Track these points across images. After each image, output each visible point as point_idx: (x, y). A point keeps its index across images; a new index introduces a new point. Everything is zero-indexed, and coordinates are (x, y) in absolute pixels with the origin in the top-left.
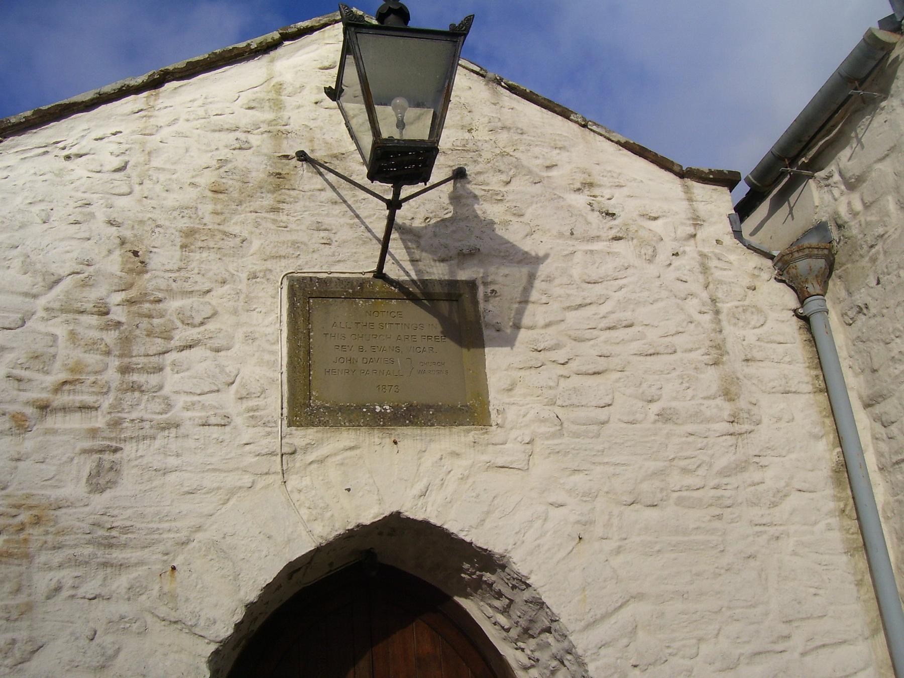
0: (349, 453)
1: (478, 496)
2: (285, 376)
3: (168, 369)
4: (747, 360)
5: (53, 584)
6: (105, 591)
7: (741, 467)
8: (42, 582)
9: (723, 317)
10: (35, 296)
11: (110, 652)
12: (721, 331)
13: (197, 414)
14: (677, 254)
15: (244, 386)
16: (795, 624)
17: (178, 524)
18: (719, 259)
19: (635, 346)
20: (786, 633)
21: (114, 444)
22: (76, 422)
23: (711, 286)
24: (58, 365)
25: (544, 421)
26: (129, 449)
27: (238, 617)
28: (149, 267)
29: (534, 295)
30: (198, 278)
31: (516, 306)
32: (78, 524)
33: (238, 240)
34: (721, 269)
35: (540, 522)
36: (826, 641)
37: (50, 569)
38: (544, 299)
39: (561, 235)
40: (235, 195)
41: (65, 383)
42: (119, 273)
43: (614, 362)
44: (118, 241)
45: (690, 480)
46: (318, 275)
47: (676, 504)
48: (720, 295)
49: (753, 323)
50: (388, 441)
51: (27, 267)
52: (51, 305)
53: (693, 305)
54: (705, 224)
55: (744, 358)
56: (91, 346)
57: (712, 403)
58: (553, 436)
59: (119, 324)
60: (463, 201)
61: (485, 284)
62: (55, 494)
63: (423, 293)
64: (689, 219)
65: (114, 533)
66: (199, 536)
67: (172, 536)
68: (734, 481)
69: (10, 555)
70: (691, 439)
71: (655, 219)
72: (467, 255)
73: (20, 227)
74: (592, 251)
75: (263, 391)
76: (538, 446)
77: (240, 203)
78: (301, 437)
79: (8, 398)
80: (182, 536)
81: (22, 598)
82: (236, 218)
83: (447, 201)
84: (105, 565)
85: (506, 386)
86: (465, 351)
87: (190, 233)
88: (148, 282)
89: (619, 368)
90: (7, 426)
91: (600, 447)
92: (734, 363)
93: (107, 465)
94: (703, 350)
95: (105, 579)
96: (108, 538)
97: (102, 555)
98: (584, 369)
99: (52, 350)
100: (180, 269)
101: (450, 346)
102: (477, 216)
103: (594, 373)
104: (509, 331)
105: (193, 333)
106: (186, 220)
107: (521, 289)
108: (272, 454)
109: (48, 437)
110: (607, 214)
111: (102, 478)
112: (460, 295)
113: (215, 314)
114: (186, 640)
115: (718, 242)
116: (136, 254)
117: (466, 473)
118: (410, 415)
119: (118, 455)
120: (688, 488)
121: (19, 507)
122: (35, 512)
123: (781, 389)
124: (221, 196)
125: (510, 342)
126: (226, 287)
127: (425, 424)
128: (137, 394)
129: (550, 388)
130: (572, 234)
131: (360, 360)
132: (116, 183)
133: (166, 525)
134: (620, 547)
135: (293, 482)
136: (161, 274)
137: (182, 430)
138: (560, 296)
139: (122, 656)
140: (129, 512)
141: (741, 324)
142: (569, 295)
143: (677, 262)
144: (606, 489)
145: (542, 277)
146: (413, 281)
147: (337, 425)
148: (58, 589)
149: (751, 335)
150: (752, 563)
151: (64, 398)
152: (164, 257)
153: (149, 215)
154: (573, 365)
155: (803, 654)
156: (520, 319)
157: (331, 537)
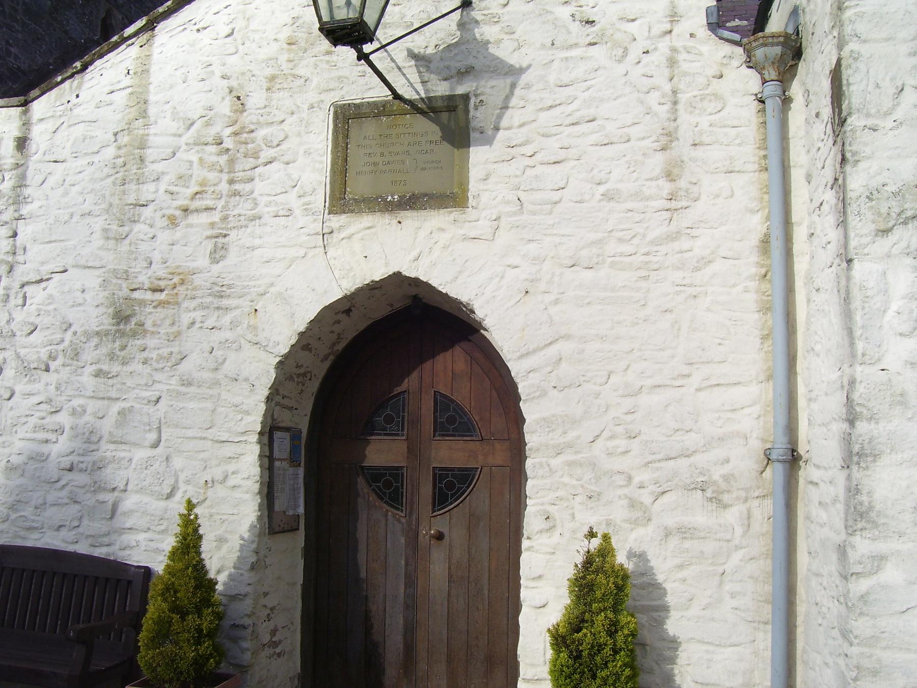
0: (368, 231)
1: (454, 260)
2: (328, 178)
3: (257, 179)
4: (695, 145)
5: (191, 320)
6: (217, 324)
7: (674, 237)
8: (186, 319)
9: (680, 107)
10: (180, 136)
11: (220, 361)
12: (675, 120)
13: (272, 209)
14: (647, 52)
15: (302, 187)
16: (695, 366)
17: (260, 282)
18: (688, 52)
19: (593, 138)
20: (686, 372)
21: (224, 232)
22: (204, 219)
23: (675, 79)
24: (193, 181)
25: (508, 203)
26: (233, 234)
27: (293, 341)
28: (246, 107)
29: (514, 102)
30: (276, 112)
31: (498, 111)
32: (204, 283)
33: (303, 80)
34: (690, 61)
35: (498, 279)
36: (721, 381)
37: (190, 311)
38: (522, 104)
39: (543, 46)
40: (303, 44)
41: (197, 193)
42: (229, 114)
43: (572, 153)
44: (228, 90)
45: (627, 248)
46: (354, 102)
47: (610, 267)
48: (682, 86)
49: (709, 110)
50: (395, 222)
51: (175, 116)
52: (189, 141)
53: (655, 97)
54: (682, 19)
55: (691, 142)
56: (212, 167)
57: (654, 183)
58: (515, 214)
59: (228, 150)
60: (467, 26)
61: (476, 96)
62: (192, 265)
63: (428, 108)
64: (666, 17)
65: (224, 289)
66: (272, 290)
67: (255, 289)
68: (663, 249)
69: (169, 303)
70: (630, 214)
71: (633, 20)
72: (466, 72)
73: (170, 88)
74: (567, 58)
75: (314, 190)
76: (503, 222)
77: (305, 51)
78: (336, 221)
79: (166, 206)
80: (261, 290)
81: (175, 329)
82: (304, 63)
83: (456, 28)
84: (218, 308)
85: (481, 177)
86: (456, 150)
87: (272, 78)
88: (247, 119)
89: (576, 157)
90: (166, 223)
91: (551, 222)
92: (681, 148)
93: (220, 246)
94: (654, 138)
95: (218, 317)
96: (220, 291)
97: (217, 302)
98: (546, 160)
99: (190, 172)
100: (265, 107)
101: (446, 146)
102: (475, 39)
103: (555, 163)
104: (490, 132)
105: (272, 153)
106: (270, 69)
107: (504, 96)
108: (317, 234)
109: (188, 229)
110: (587, 22)
111: (218, 254)
112: (457, 107)
113: (286, 137)
114: (263, 355)
115: (692, 35)
116: (239, 98)
117: (447, 244)
118: (412, 202)
119: (227, 239)
120: (621, 255)
121: (173, 274)
122: (181, 277)
123: (725, 169)
124: (293, 47)
125: (489, 141)
126: (295, 116)
127: (421, 209)
128: (237, 198)
129: (516, 176)
130: (553, 44)
131: (381, 164)
132: (227, 46)
133: (252, 283)
134: (557, 299)
135: (331, 252)
136: (254, 111)
137: (263, 221)
138: (535, 100)
139: (227, 363)
140: (233, 275)
141: (697, 111)
142: (542, 99)
143: (646, 59)
144: (552, 255)
145: (522, 86)
146: (422, 99)
147: (360, 212)
148: (193, 323)
149: (704, 121)
150: (668, 315)
151: (197, 204)
152: (255, 100)
153: (248, 68)
154: (538, 157)
155: (698, 390)
156: (499, 123)
157: (353, 290)
